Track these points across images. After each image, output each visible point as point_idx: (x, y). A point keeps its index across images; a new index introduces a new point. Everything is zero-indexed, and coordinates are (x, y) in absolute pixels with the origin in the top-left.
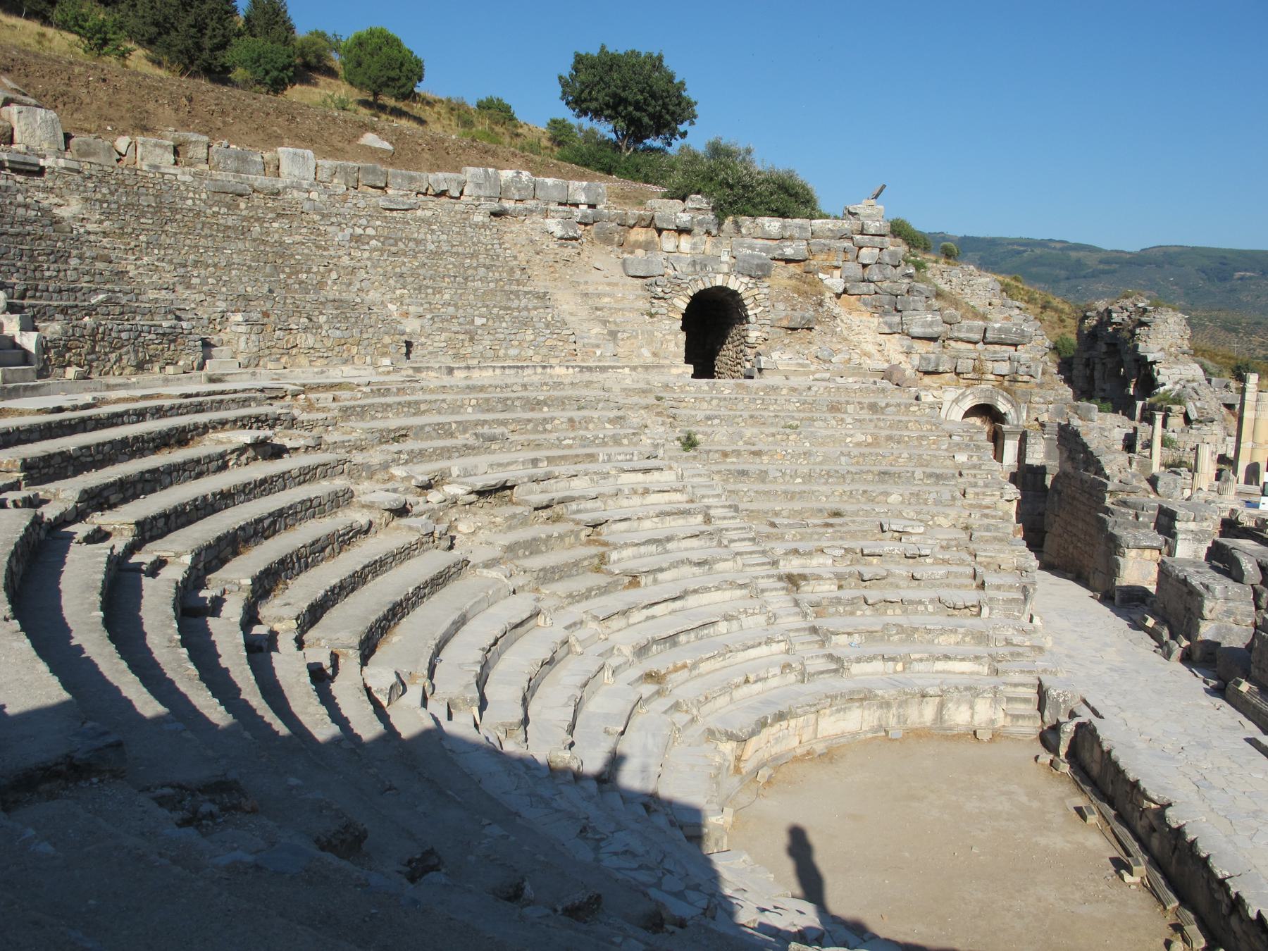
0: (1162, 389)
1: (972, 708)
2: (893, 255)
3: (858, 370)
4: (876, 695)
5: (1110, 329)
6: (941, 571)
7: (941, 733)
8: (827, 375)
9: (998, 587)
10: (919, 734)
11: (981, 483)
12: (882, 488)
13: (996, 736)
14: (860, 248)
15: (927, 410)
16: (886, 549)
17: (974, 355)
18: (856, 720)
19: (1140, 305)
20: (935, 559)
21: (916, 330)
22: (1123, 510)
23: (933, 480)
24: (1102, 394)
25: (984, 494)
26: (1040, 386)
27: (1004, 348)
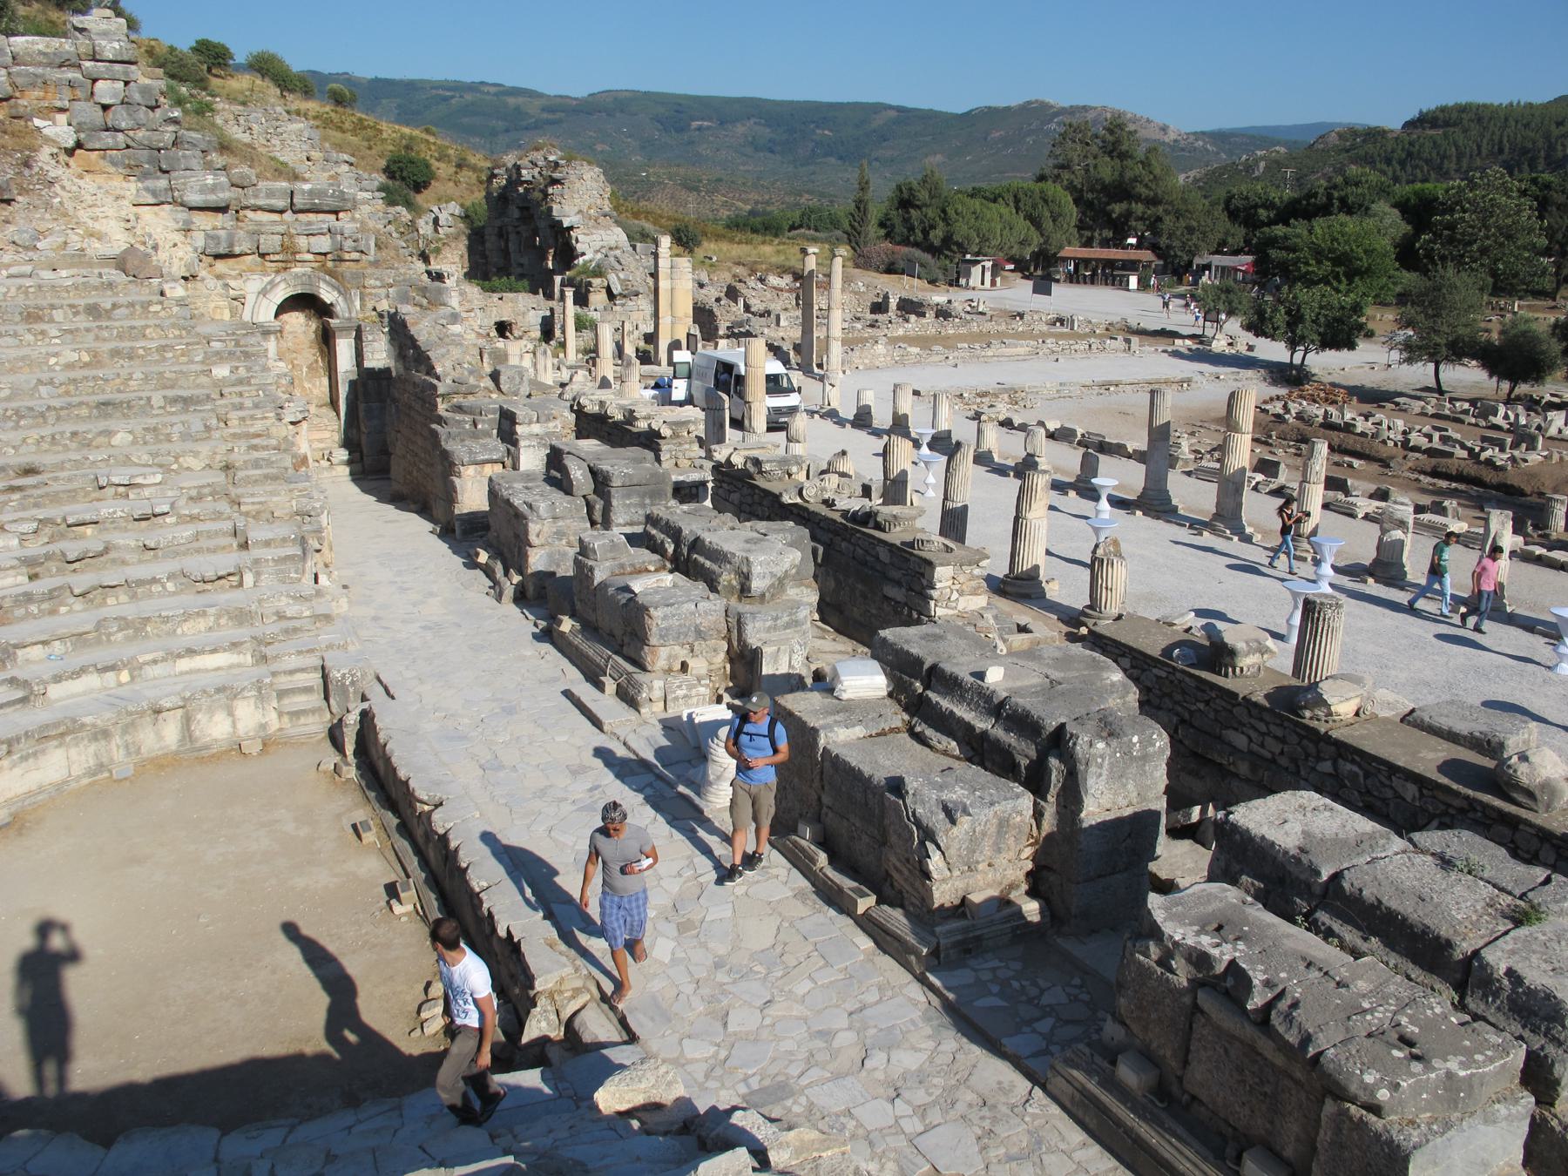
1: (231, 714)
2: (145, 90)
3: (80, 258)
4: (83, 725)
5: (521, 190)
6: (187, 532)
7: (193, 754)
8: (28, 269)
9: (267, 544)
10: (163, 764)
11: (248, 403)
12: (102, 425)
13: (268, 744)
14: (95, 81)
15: (175, 309)
16: (104, 512)
17: (281, 229)
18: (57, 765)
19: (552, 158)
20: (180, 516)
21: (194, 198)
22: (458, 417)
23: (179, 406)
24: (519, 270)
25: (252, 418)
26: (376, 264)
27: (321, 216)
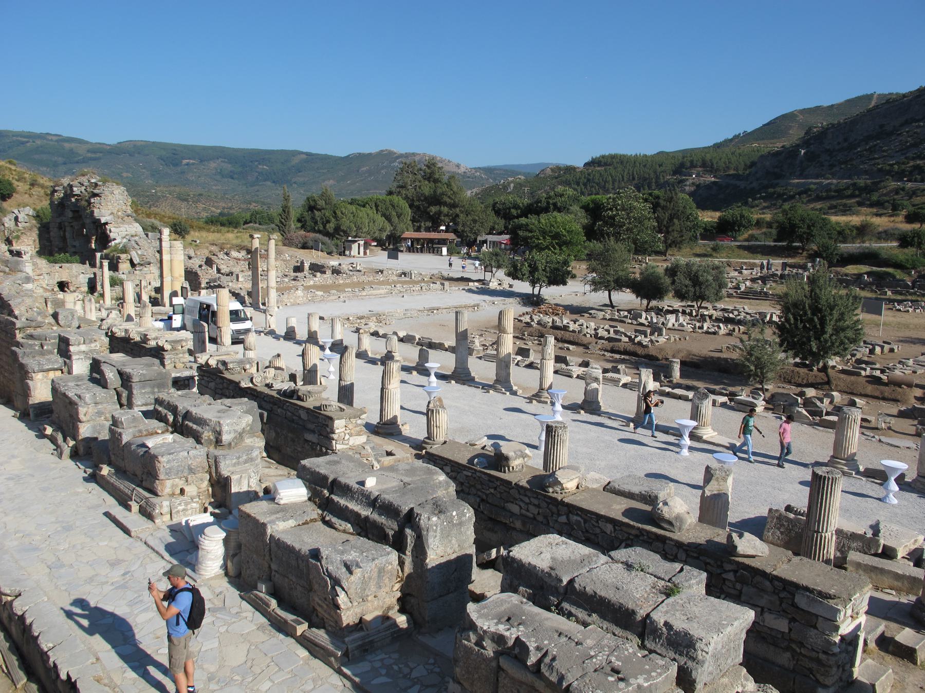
0: (113, 243)
5: (73, 200)
19: (93, 181)
22: (31, 342)
24: (73, 250)
